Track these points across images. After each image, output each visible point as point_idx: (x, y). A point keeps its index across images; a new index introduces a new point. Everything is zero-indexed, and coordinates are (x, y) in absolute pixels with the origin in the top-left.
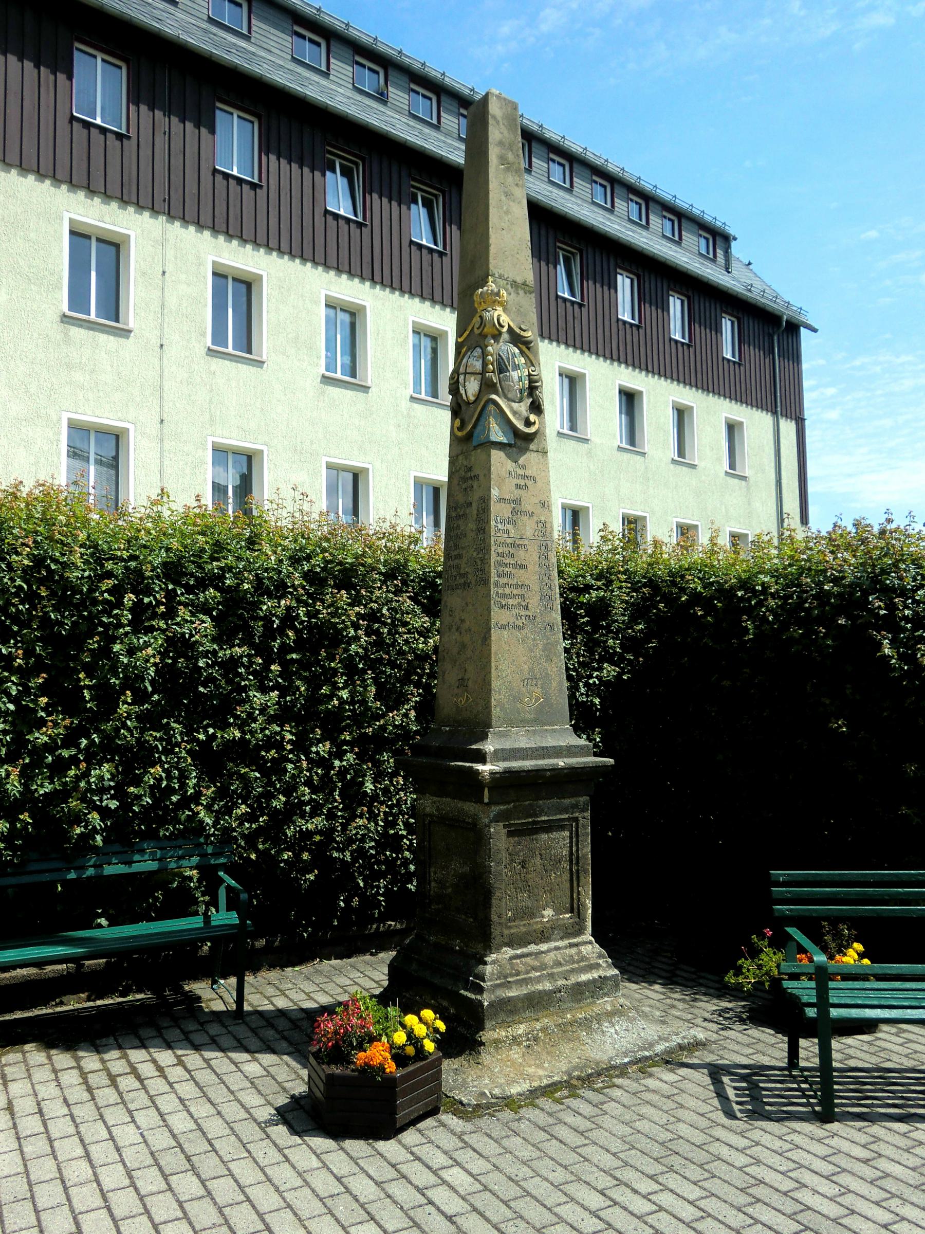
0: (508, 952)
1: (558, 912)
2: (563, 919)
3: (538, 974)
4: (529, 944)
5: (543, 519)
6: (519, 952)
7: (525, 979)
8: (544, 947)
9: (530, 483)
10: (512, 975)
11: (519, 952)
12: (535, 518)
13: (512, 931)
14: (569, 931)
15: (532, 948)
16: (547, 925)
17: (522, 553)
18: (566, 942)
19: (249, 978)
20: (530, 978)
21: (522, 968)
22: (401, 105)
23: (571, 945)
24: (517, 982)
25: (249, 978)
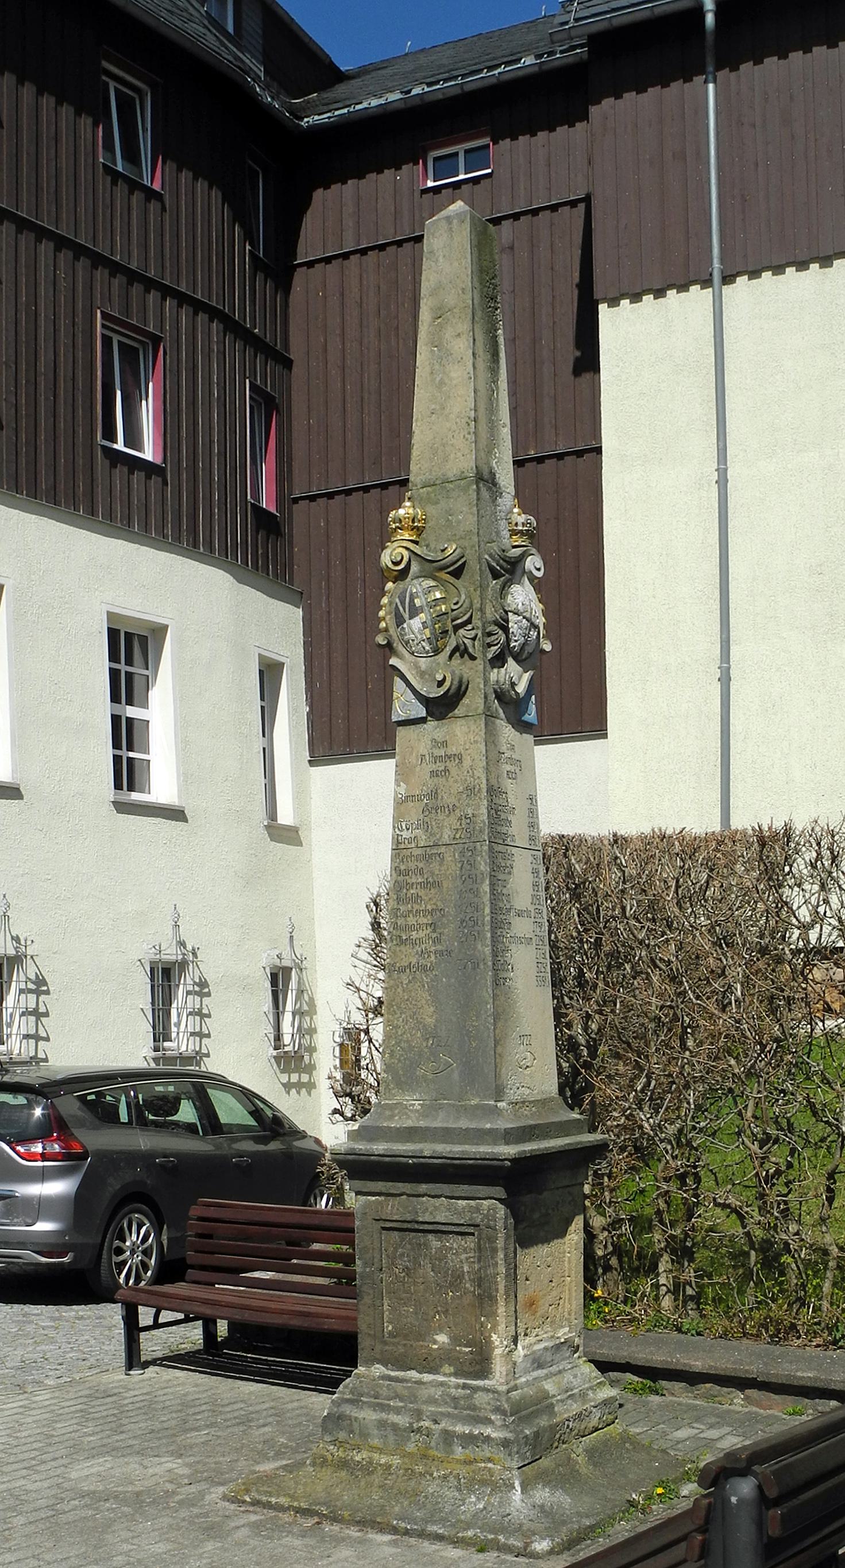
0: (378, 1370)
1: (455, 1340)
2: (460, 1352)
3: (401, 1404)
4: (410, 1369)
5: (470, 812)
6: (393, 1374)
7: (381, 1404)
8: (427, 1377)
9: (452, 765)
10: (368, 1395)
11: (393, 1374)
12: (458, 813)
13: (387, 1348)
14: (466, 1369)
15: (413, 1374)
16: (434, 1354)
17: (435, 866)
18: (461, 1381)
19: (717, 828)
20: (389, 1405)
21: (384, 1392)
22: (349, 223)
23: (465, 1386)
24: (370, 1405)
25: (717, 828)
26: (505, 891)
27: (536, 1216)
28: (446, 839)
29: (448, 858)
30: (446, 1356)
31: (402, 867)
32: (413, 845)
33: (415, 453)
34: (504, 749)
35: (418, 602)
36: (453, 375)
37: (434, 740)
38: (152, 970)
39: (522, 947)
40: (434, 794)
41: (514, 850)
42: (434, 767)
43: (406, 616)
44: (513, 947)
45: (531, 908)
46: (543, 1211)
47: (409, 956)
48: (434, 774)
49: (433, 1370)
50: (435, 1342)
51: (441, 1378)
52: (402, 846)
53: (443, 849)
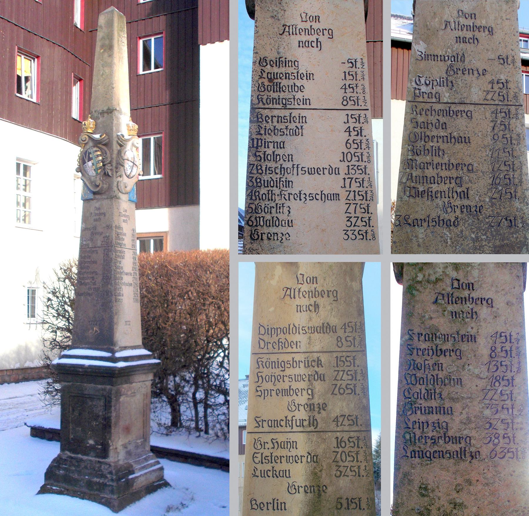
1: (97, 443)
5: (107, 234)
9: (102, 217)
15: (80, 456)
18: (97, 459)
26: (120, 265)
27: (129, 393)
28: (475, 98)
29: (99, 252)
30: (92, 448)
31: (83, 255)
32: (434, 100)
33: (126, 42)
34: (122, 211)
35: (91, 156)
36: (107, 71)
37: (95, 207)
38: (28, 290)
39: (127, 287)
40: (95, 228)
41: (125, 250)
42: (95, 218)
43: (87, 161)
44: (123, 287)
45: (132, 272)
46: (133, 391)
47: (84, 289)
48: (95, 220)
49: (87, 454)
50: (88, 443)
51: (90, 458)
52: (421, 99)
53: (97, 249)
